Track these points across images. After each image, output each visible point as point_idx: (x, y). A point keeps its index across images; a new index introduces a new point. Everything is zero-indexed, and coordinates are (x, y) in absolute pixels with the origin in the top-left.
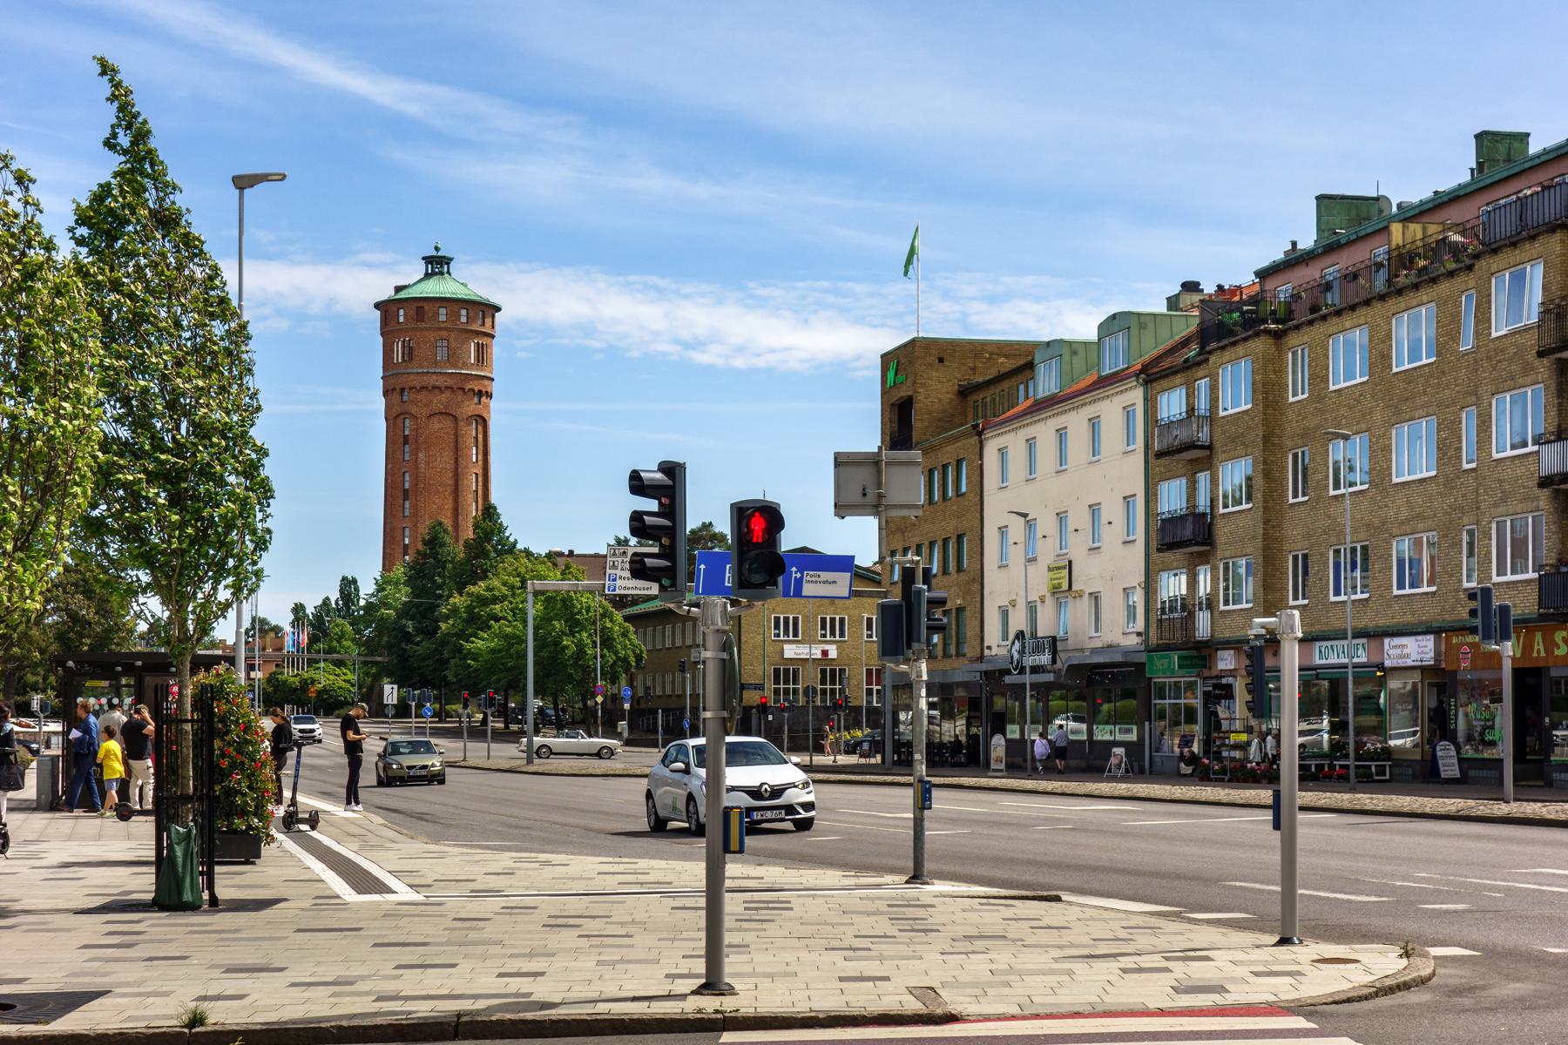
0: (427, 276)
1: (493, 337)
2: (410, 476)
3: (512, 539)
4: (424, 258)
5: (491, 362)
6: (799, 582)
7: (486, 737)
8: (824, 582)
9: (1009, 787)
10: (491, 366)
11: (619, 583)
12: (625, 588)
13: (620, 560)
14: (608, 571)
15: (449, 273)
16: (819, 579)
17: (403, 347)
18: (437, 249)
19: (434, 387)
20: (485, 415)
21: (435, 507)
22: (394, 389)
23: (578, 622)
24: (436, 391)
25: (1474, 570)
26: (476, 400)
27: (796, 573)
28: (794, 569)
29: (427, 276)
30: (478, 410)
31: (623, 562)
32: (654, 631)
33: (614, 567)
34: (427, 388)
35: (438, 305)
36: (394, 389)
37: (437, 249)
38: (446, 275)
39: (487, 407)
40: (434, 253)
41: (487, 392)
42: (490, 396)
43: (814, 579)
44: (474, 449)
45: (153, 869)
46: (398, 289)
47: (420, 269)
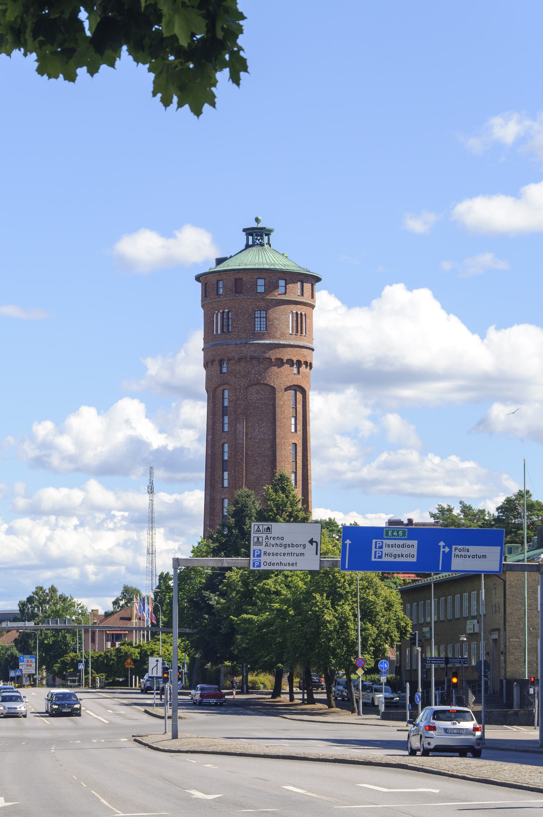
0: (248, 246)
1: (313, 307)
4: (245, 230)
5: (311, 331)
6: (448, 557)
7: (481, 703)
8: (473, 557)
9: (370, 759)
10: (311, 335)
11: (263, 558)
12: (270, 564)
13: (264, 536)
14: (253, 547)
16: (467, 554)
18: (257, 220)
19: (252, 358)
21: (253, 477)
22: (213, 361)
23: (341, 596)
24: (255, 362)
26: (295, 370)
27: (444, 547)
28: (442, 544)
29: (248, 246)
30: (298, 380)
31: (267, 538)
32: (418, 605)
33: (258, 542)
34: (246, 358)
36: (213, 361)
37: (257, 220)
38: (266, 246)
39: (307, 376)
40: (255, 225)
43: (463, 553)
44: (293, 420)
46: (219, 261)
47: (242, 239)
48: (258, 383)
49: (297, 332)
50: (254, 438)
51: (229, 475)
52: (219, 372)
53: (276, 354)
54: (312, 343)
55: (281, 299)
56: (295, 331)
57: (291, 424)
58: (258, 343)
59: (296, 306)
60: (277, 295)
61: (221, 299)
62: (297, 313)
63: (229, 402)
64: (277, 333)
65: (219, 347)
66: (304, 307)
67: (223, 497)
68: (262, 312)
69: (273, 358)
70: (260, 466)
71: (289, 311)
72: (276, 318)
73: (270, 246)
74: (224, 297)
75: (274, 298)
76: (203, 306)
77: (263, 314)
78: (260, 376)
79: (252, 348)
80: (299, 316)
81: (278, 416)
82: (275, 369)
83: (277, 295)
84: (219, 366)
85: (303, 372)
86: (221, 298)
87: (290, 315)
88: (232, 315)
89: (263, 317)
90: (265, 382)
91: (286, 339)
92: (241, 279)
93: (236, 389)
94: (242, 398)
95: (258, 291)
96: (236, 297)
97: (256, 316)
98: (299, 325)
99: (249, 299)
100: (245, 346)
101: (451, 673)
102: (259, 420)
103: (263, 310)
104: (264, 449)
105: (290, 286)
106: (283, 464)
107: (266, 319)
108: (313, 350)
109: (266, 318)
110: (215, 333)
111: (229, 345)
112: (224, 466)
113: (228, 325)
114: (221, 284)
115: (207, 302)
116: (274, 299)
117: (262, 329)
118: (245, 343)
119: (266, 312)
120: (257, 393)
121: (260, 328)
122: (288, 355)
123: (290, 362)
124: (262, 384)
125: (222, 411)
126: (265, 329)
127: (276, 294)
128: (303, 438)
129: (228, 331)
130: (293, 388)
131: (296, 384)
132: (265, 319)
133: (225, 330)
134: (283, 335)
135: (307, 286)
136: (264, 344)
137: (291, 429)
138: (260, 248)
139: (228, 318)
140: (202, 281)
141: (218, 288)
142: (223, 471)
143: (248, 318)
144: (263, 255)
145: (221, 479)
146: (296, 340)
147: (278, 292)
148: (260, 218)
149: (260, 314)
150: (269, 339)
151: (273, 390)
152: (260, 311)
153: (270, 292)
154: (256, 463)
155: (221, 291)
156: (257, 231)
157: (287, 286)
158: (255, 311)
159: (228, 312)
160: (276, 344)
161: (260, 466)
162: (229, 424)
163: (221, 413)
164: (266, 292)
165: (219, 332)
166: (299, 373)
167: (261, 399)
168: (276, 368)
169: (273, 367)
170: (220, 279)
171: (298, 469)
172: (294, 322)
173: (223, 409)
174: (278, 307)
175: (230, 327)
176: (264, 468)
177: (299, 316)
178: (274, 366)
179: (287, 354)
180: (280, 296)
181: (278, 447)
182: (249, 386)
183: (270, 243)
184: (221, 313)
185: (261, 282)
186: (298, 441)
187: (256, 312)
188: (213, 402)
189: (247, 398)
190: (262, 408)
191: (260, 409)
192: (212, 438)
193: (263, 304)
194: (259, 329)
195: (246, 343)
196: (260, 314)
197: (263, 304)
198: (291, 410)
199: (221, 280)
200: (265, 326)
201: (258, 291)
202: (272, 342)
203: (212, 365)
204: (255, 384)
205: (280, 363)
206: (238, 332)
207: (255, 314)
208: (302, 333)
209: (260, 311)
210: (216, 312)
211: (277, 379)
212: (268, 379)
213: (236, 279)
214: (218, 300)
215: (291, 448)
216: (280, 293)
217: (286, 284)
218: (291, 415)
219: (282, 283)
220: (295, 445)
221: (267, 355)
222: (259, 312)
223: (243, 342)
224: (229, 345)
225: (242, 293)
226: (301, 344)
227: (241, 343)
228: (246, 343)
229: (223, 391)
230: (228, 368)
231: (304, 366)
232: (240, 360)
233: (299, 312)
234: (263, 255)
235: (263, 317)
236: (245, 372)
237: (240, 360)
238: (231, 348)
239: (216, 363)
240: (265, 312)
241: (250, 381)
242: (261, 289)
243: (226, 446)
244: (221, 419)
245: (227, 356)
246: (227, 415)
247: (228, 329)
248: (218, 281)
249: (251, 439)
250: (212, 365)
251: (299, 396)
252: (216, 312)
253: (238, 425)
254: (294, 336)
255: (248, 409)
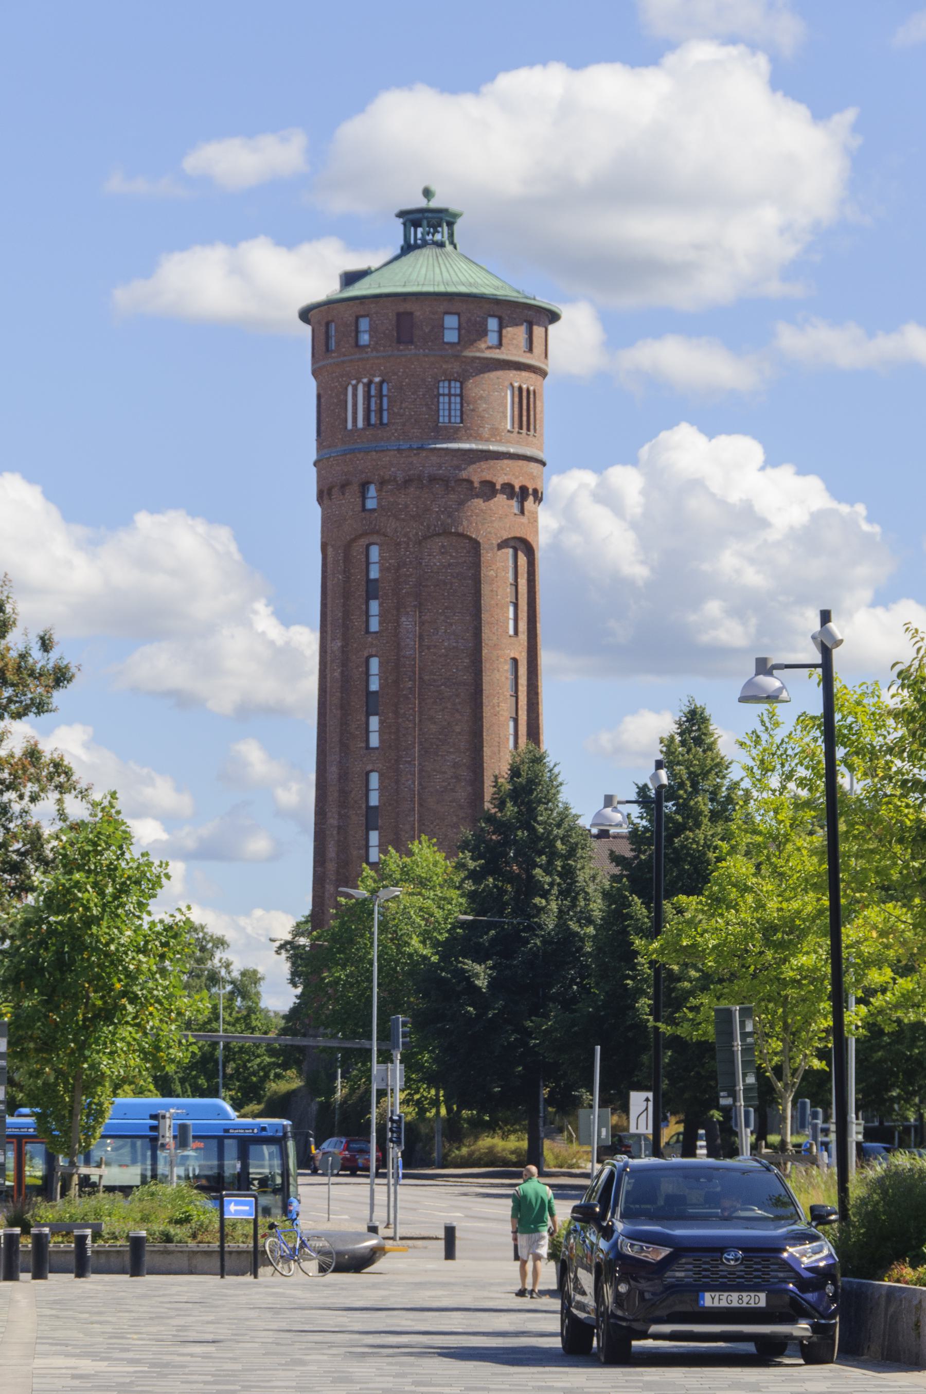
0: (408, 248)
2: (381, 664)
3: (560, 779)
9: (371, 1336)
15: (452, 243)
17: (368, 397)
18: (427, 193)
19: (433, 479)
20: (530, 539)
22: (344, 486)
24: (438, 488)
25: (225, 1008)
29: (408, 248)
35: (441, 309)
36: (344, 486)
37: (427, 193)
38: (449, 248)
39: (534, 520)
40: (422, 203)
41: (535, 491)
42: (538, 497)
44: (511, 609)
45: (559, 1316)
46: (350, 278)
48: (446, 533)
49: (521, 427)
50: (435, 646)
51: (381, 722)
52: (358, 508)
53: (482, 471)
54: (541, 450)
55: (491, 359)
56: (516, 426)
57: (508, 619)
58: (447, 449)
59: (519, 372)
60: (484, 349)
61: (365, 355)
62: (520, 389)
63: (381, 571)
64: (484, 427)
65: (360, 456)
66: (533, 375)
67: (369, 768)
68: (453, 384)
69: (476, 480)
70: (449, 705)
71: (507, 383)
72: (481, 398)
73: (455, 247)
74: (372, 351)
75: (478, 354)
76: (314, 373)
77: (456, 388)
78: (449, 516)
79: (434, 459)
80: (525, 394)
81: (485, 601)
82: (478, 503)
83: (484, 349)
84: (359, 495)
85: (529, 512)
86: (367, 353)
87: (509, 393)
88: (389, 390)
89: (455, 395)
90: (460, 530)
91: (500, 441)
92: (411, 314)
93: (399, 544)
94: (411, 562)
95: (446, 340)
96: (399, 350)
97: (441, 391)
98: (525, 413)
99: (427, 356)
100: (419, 454)
101: (868, 1144)
102: (447, 608)
103: (456, 380)
104: (457, 669)
105: (509, 331)
106: (495, 701)
107: (462, 399)
108: (544, 464)
109: (461, 396)
110: (350, 425)
111: (383, 451)
112: (371, 703)
113: (380, 410)
114: (364, 324)
115: (330, 361)
116: (479, 358)
117: (453, 420)
118: (418, 448)
119: (462, 384)
120: (443, 553)
121: (450, 416)
122: (506, 474)
123: (508, 489)
124: (451, 533)
125: (365, 589)
126: (458, 420)
127: (483, 346)
128: (529, 648)
129: (381, 423)
130: (512, 543)
131: (518, 535)
132: (458, 399)
133: (373, 421)
134: (495, 433)
135: (538, 331)
136: (459, 450)
137: (507, 627)
138: (438, 250)
139: (380, 396)
140: (313, 320)
141: (357, 332)
142: (368, 715)
143: (424, 395)
144: (448, 265)
145: (364, 732)
146: (518, 443)
147: (485, 342)
148: (433, 188)
149: (450, 388)
150: (468, 440)
151: (475, 546)
152: (450, 381)
153: (472, 342)
154: (440, 699)
155: (365, 338)
156: (430, 215)
157: (504, 332)
158: (439, 381)
159: (382, 383)
160: (482, 451)
161: (449, 705)
162: (380, 615)
163: (364, 593)
164: (462, 343)
165: (360, 424)
166: (522, 512)
167: (450, 565)
168: (480, 501)
169: (476, 500)
170: (362, 313)
171: (520, 712)
172: (516, 406)
173: (367, 586)
174: (486, 375)
175: (385, 414)
176: (457, 710)
177: (525, 394)
178: (477, 496)
179: (503, 473)
180: (490, 351)
181: (486, 665)
182: (425, 538)
183: (456, 240)
184: (364, 384)
185: (451, 321)
186: (521, 653)
187: (441, 384)
188: (345, 571)
189: (421, 563)
190: (451, 583)
191: (449, 586)
192: (343, 647)
193: (456, 368)
194: (447, 420)
195: (421, 448)
196: (450, 388)
197: (456, 368)
198: (508, 590)
199: (367, 316)
200: (458, 413)
201: (446, 340)
202: (474, 446)
203: (343, 494)
204: (439, 535)
205: (489, 490)
206: (404, 425)
207: (438, 388)
208: (528, 429)
209: (450, 381)
210: (354, 382)
211: (483, 524)
212: (465, 523)
213: (399, 315)
214: (357, 356)
215: (508, 667)
216: (490, 344)
217: (501, 327)
218: (509, 600)
219: (493, 324)
220: (515, 661)
221: (464, 475)
222: (446, 384)
223: (415, 446)
224: (383, 451)
225: (411, 342)
226: (528, 451)
227: (411, 449)
228: (421, 448)
229: (368, 547)
230: (379, 499)
231: (531, 498)
232: (407, 482)
233: (524, 387)
234: (448, 265)
235: (455, 395)
236: (417, 507)
237: (407, 482)
238: (388, 458)
239: (355, 488)
240: (458, 384)
241: (429, 528)
242: (451, 336)
243: (374, 664)
244: (364, 607)
245: (379, 475)
246: (376, 598)
247: (381, 418)
248: (357, 318)
249: (429, 648)
250: (343, 494)
251: (522, 560)
252: (354, 382)
253: (403, 619)
254: (515, 435)
255: (424, 586)
